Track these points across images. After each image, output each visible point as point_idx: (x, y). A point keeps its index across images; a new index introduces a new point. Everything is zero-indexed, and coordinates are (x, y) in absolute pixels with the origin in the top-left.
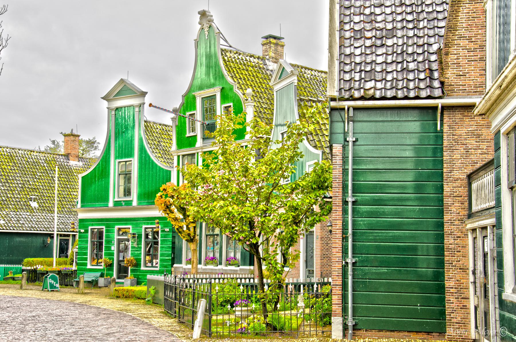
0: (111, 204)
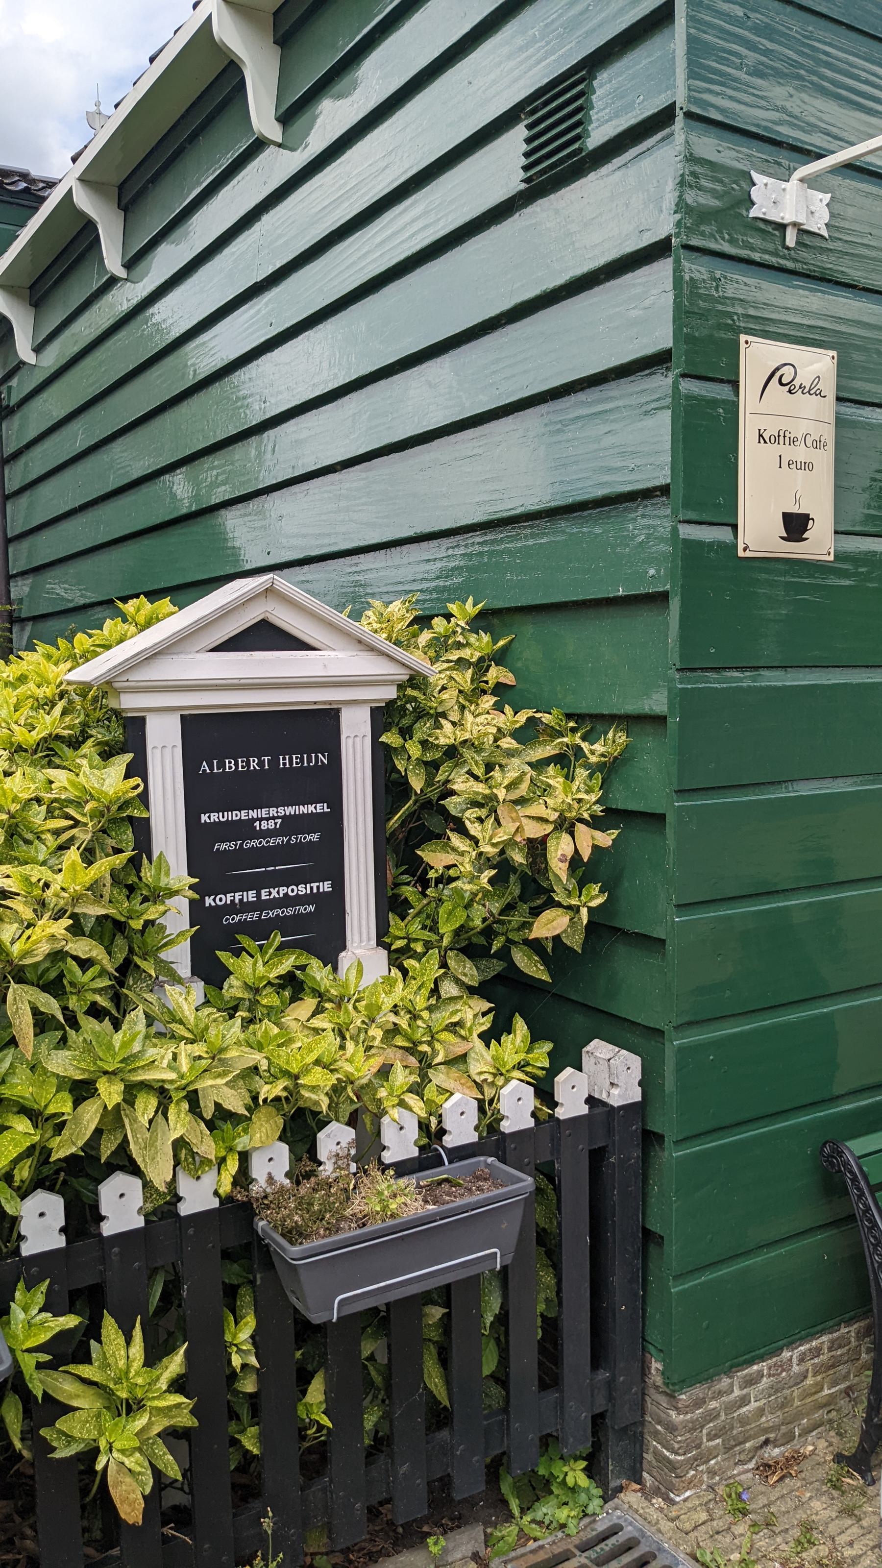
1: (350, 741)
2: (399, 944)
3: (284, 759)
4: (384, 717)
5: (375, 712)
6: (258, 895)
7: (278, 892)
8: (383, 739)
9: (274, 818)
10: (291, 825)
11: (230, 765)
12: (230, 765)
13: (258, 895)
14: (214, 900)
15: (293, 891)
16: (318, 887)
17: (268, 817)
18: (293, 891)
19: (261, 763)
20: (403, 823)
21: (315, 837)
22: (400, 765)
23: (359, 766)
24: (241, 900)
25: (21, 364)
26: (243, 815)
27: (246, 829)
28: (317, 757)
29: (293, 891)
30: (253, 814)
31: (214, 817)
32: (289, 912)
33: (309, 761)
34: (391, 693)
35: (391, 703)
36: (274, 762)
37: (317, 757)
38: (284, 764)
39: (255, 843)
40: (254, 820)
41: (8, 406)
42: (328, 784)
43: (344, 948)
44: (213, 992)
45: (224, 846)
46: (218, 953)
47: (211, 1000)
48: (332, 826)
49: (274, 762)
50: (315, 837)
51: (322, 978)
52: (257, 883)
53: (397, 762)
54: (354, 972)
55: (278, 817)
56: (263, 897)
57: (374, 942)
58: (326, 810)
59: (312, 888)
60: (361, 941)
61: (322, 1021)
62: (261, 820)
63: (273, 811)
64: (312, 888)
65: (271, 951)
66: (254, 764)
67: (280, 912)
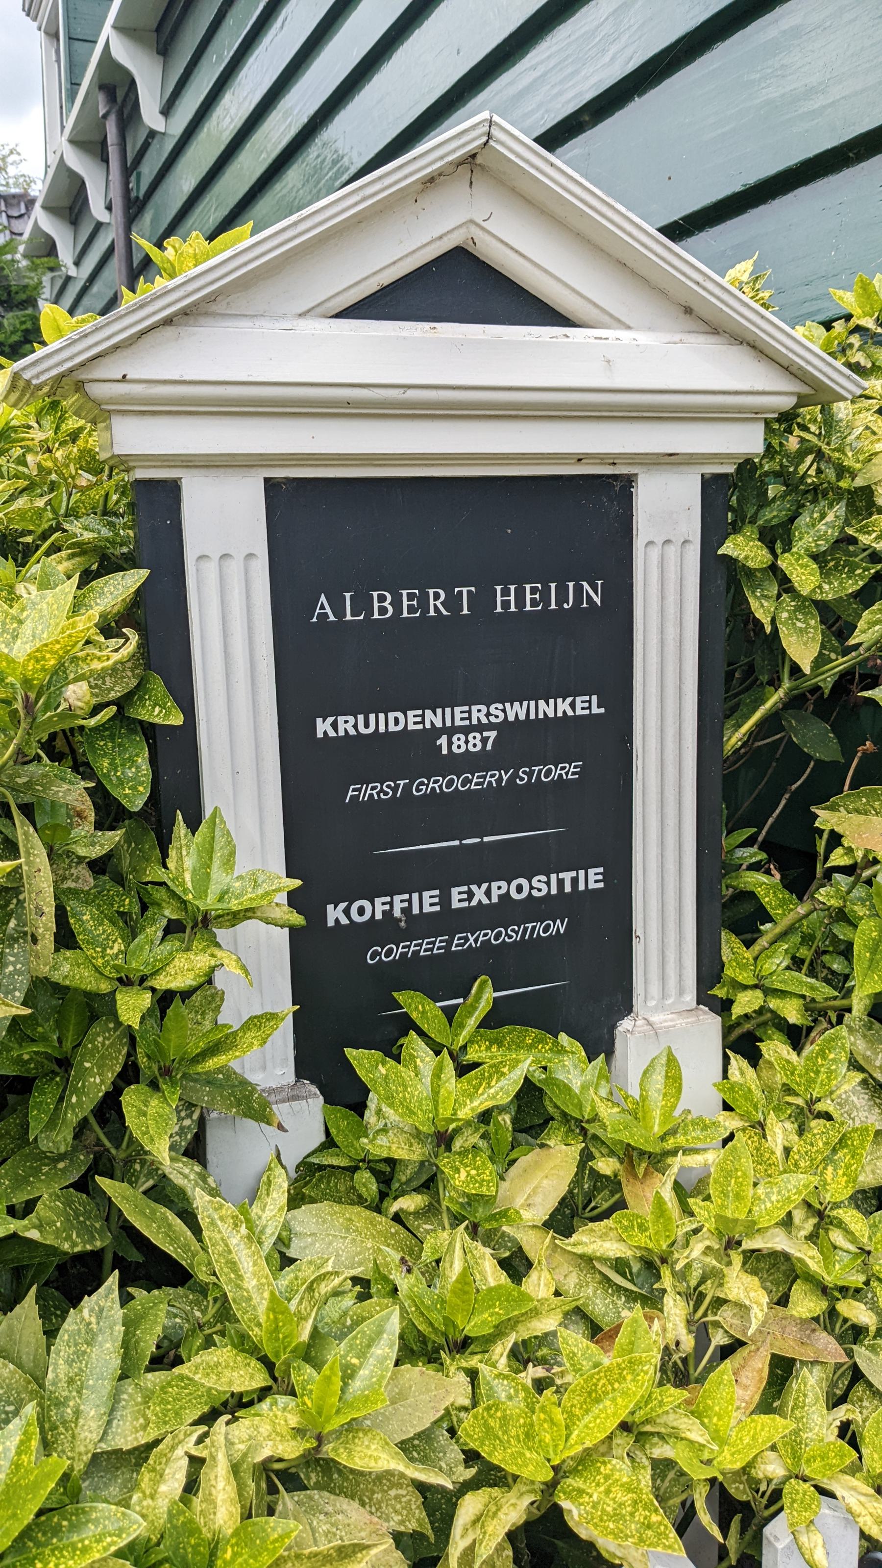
1: (654, 553)
2: (746, 1003)
3: (506, 592)
4: (729, 497)
5: (712, 487)
6: (445, 899)
7: (488, 893)
8: (728, 548)
9: (480, 728)
10: (519, 743)
11: (382, 605)
12: (382, 605)
13: (445, 899)
14: (347, 912)
15: (519, 889)
16: (575, 881)
17: (466, 726)
18: (519, 889)
19: (453, 602)
20: (753, 735)
21: (569, 771)
22: (761, 608)
23: (672, 610)
24: (407, 911)
25: (152, 134)
26: (411, 720)
27: (417, 753)
28: (579, 590)
29: (519, 889)
30: (434, 719)
31: (346, 724)
32: (512, 934)
33: (562, 597)
34: (749, 441)
35: (747, 466)
36: (482, 601)
37: (579, 590)
38: (506, 604)
39: (437, 784)
40: (437, 733)
41: (137, 198)
42: (603, 652)
43: (627, 1008)
44: (342, 1119)
45: (368, 791)
46: (351, 1053)
47: (338, 1139)
48: (610, 745)
49: (482, 601)
50: (569, 771)
51: (584, 1087)
52: (443, 873)
53: (754, 604)
54: (658, 1079)
55: (490, 726)
56: (455, 905)
57: (690, 997)
58: (595, 710)
59: (561, 883)
60: (664, 996)
61: (603, 1236)
62: (451, 731)
63: (478, 713)
64: (561, 883)
65: (472, 1022)
66: (437, 602)
67: (491, 935)
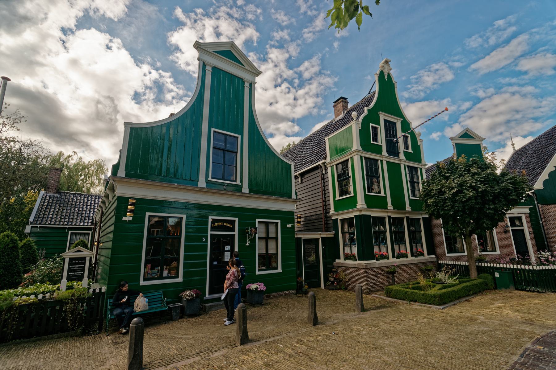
0: (202, 183)
17: (77, 266)
48: (84, 268)
